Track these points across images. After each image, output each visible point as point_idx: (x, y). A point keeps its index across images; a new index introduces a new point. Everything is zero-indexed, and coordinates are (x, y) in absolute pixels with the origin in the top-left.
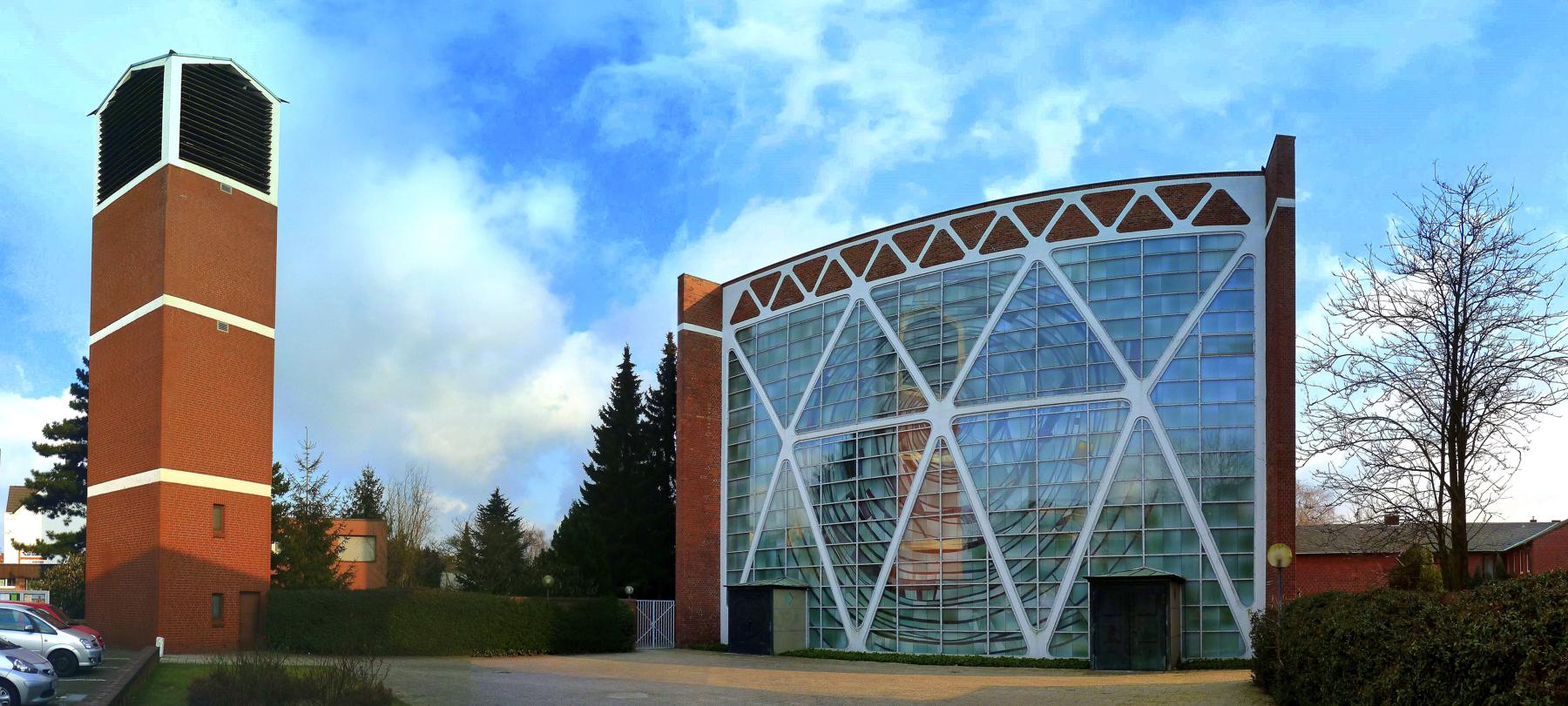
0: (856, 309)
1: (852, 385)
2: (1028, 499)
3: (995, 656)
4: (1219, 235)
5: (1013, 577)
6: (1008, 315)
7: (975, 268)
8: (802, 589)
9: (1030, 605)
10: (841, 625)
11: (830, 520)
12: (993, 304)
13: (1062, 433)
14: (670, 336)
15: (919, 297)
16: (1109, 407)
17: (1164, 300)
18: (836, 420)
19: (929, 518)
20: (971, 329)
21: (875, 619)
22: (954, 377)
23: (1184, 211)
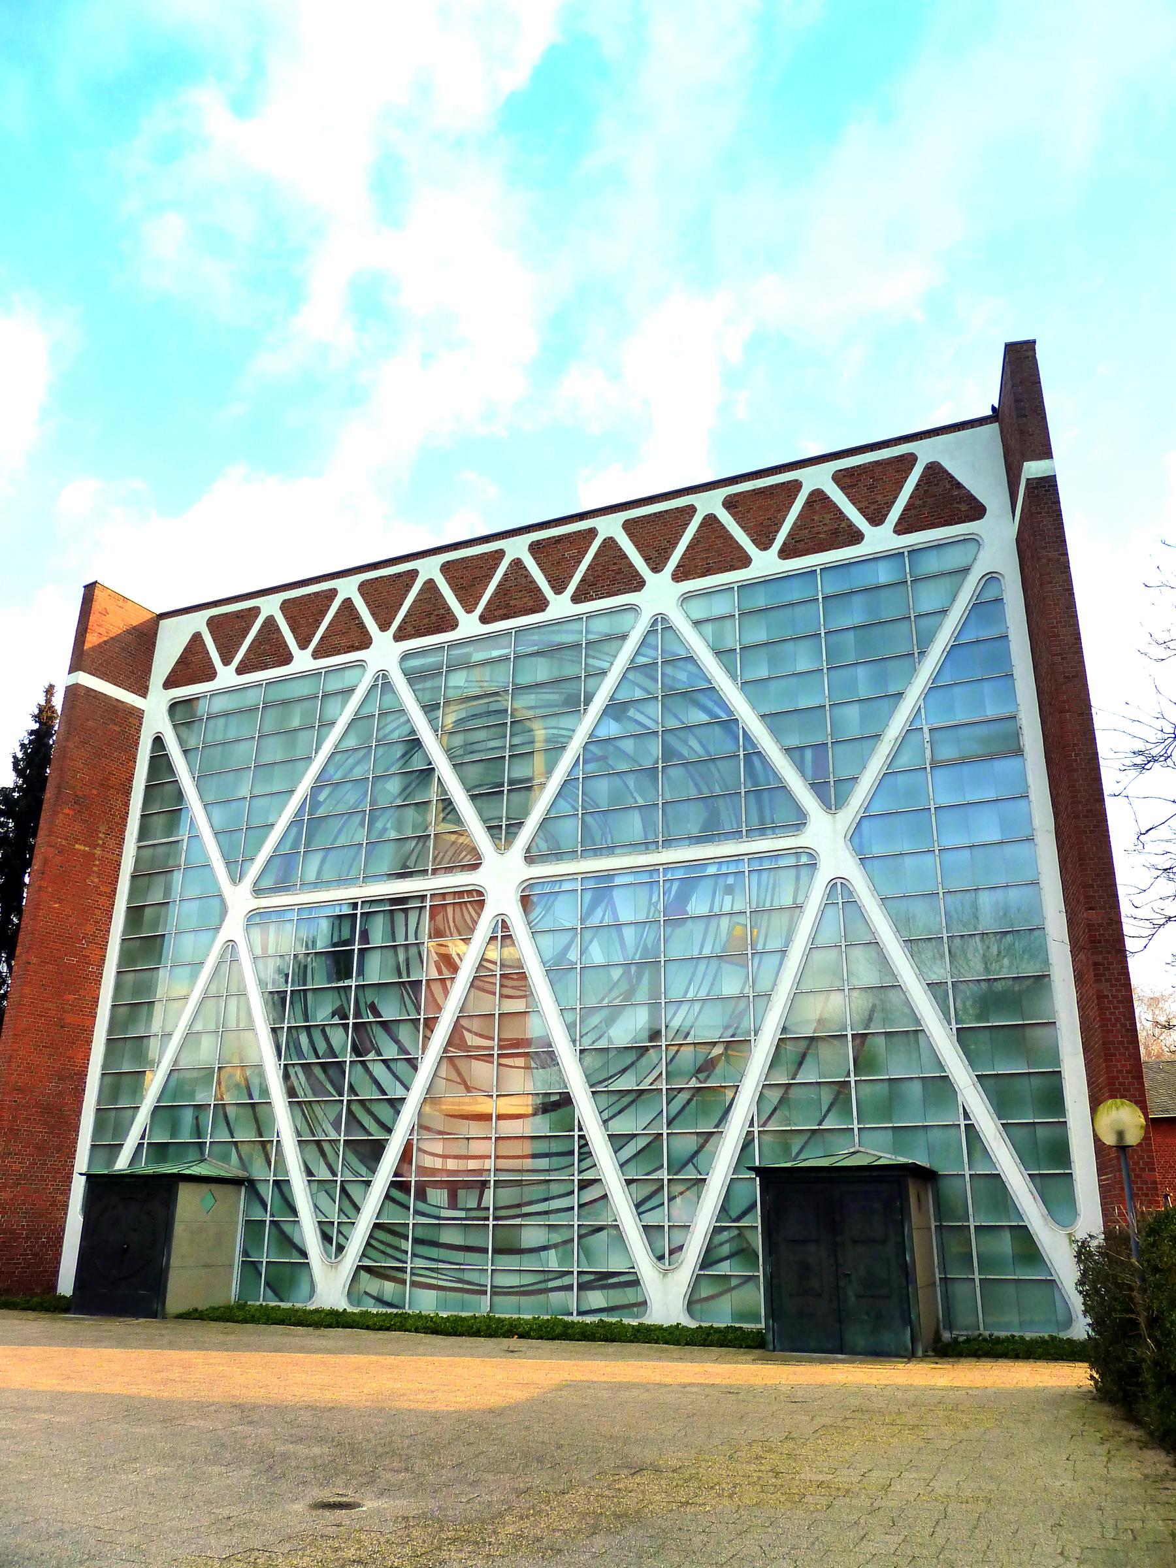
0: (374, 686)
1: (357, 819)
2: (647, 1026)
3: (588, 1319)
4: (938, 546)
5: (622, 1166)
6: (615, 709)
7: (565, 627)
8: (236, 1182)
9: (652, 1219)
10: (304, 1254)
11: (300, 1054)
12: (589, 689)
13: (703, 910)
14: (50, 691)
15: (476, 674)
16: (783, 862)
17: (861, 672)
18: (326, 876)
19: (476, 1058)
20: (555, 731)
21: (368, 1244)
22: (526, 813)
23: (879, 511)
